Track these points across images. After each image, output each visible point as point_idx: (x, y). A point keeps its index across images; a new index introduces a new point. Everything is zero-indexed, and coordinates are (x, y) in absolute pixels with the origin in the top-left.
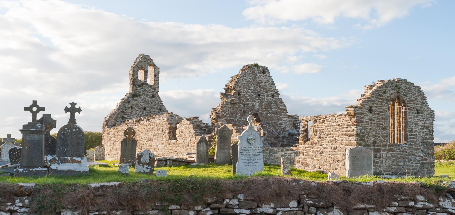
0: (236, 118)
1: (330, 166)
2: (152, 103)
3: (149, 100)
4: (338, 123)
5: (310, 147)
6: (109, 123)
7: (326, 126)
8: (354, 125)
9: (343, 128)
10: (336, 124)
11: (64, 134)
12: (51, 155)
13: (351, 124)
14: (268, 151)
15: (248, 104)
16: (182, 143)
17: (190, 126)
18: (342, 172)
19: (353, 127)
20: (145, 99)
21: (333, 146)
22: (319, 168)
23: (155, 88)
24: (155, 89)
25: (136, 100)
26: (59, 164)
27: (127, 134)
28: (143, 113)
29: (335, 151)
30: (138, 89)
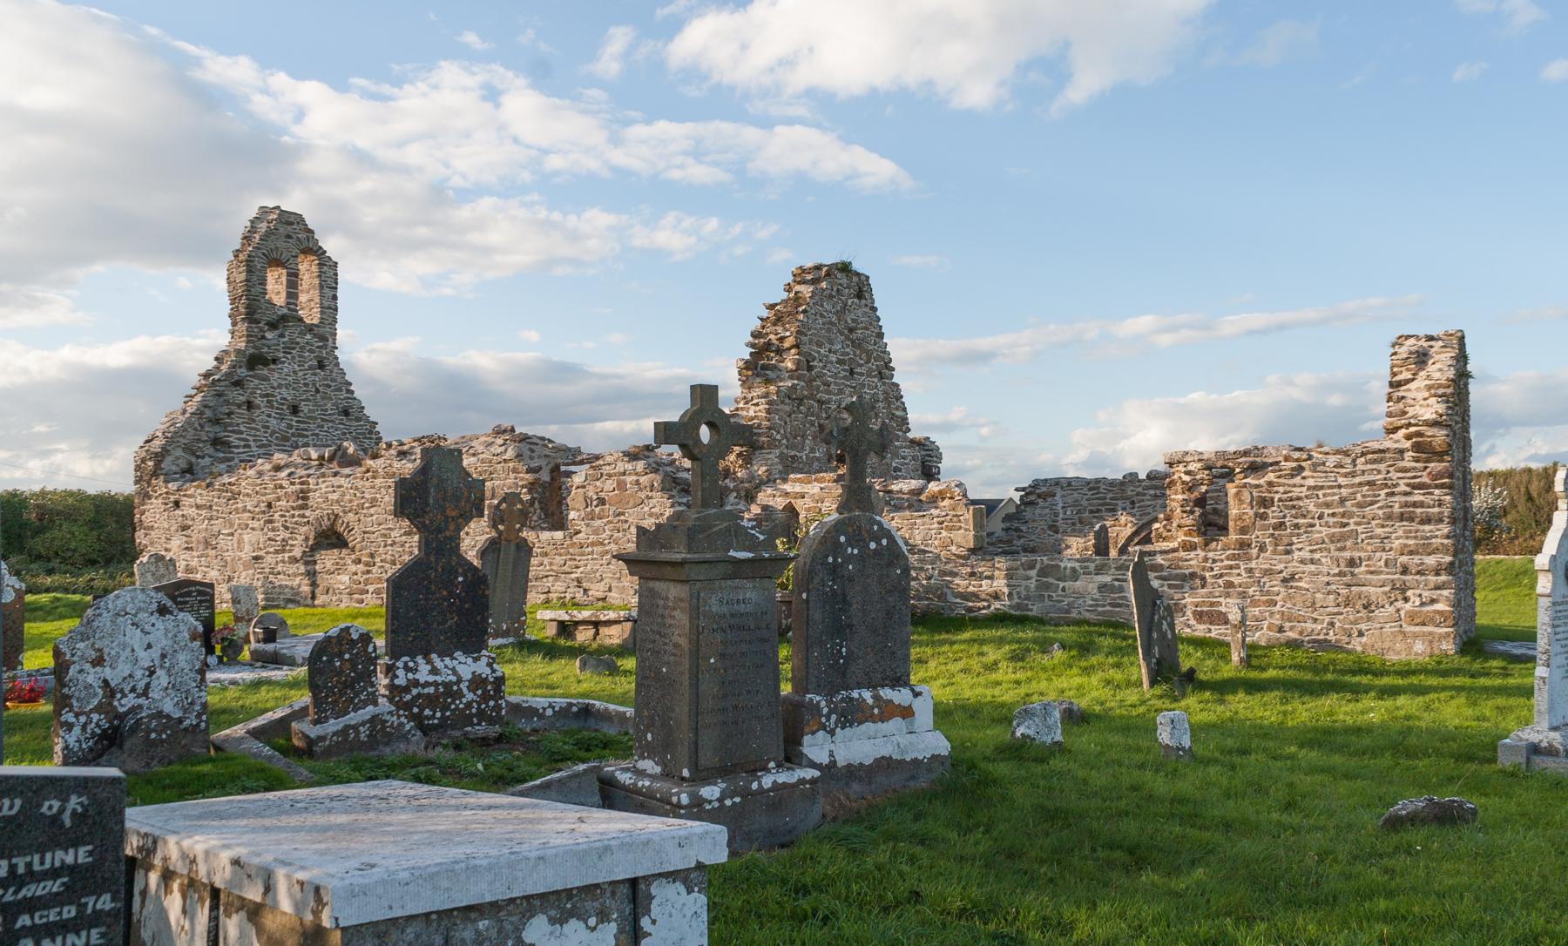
0: (803, 449)
1: (1332, 624)
2: (317, 391)
3: (310, 378)
4: (1371, 478)
5: (1234, 557)
6: (167, 464)
7: (1309, 488)
8: (1442, 486)
9: (1393, 494)
10: (1357, 480)
11: (835, 566)
12: (467, 652)
13: (1425, 480)
14: (1033, 573)
15: (829, 402)
16: (602, 544)
17: (644, 480)
18: (1386, 645)
19: (1437, 492)
20: (295, 372)
21: (1347, 554)
22: (1281, 630)
23: (324, 333)
24: (323, 339)
25: (266, 379)
26: (832, 733)
27: (502, 522)
28: (290, 427)
29: (1352, 574)
30: (269, 335)
